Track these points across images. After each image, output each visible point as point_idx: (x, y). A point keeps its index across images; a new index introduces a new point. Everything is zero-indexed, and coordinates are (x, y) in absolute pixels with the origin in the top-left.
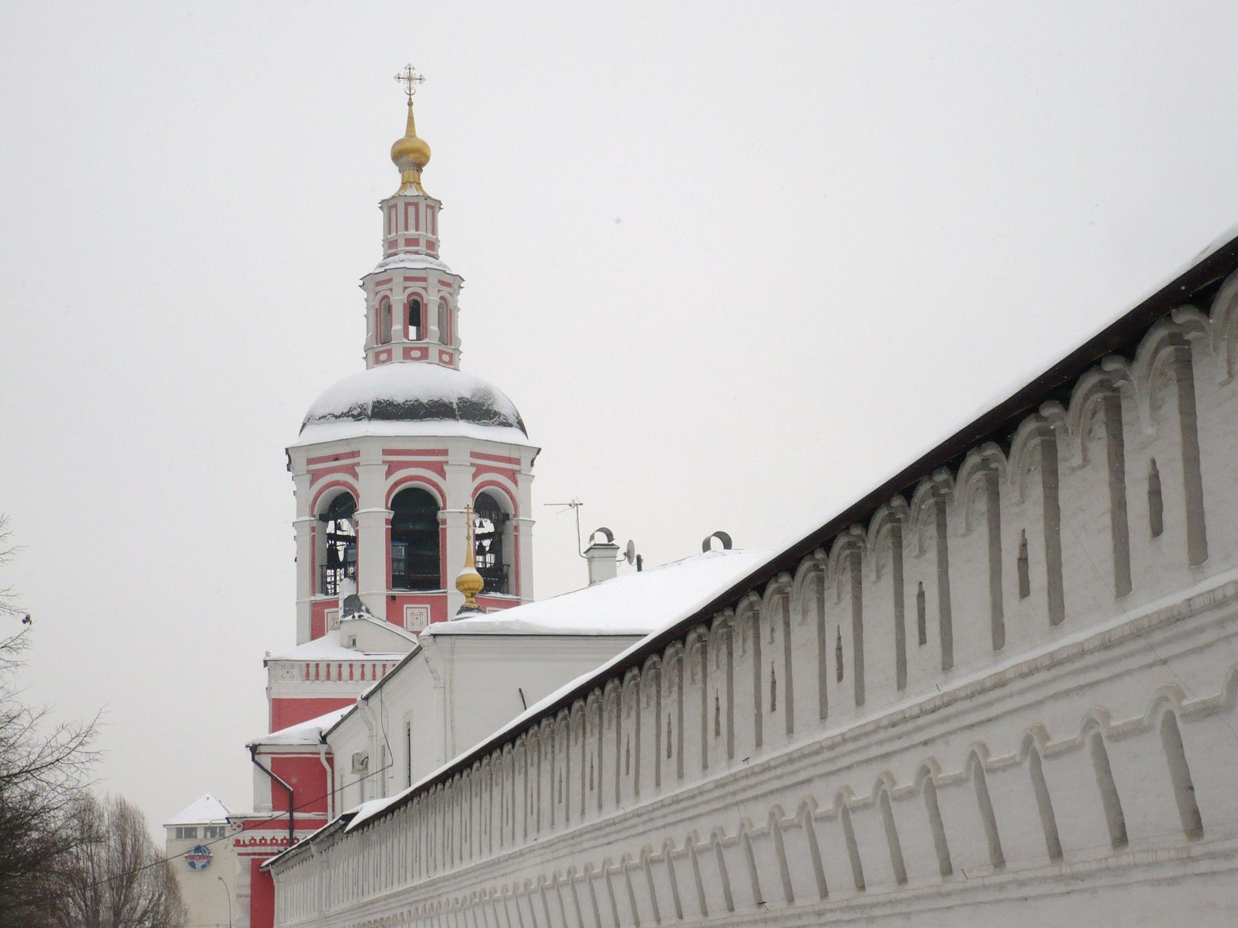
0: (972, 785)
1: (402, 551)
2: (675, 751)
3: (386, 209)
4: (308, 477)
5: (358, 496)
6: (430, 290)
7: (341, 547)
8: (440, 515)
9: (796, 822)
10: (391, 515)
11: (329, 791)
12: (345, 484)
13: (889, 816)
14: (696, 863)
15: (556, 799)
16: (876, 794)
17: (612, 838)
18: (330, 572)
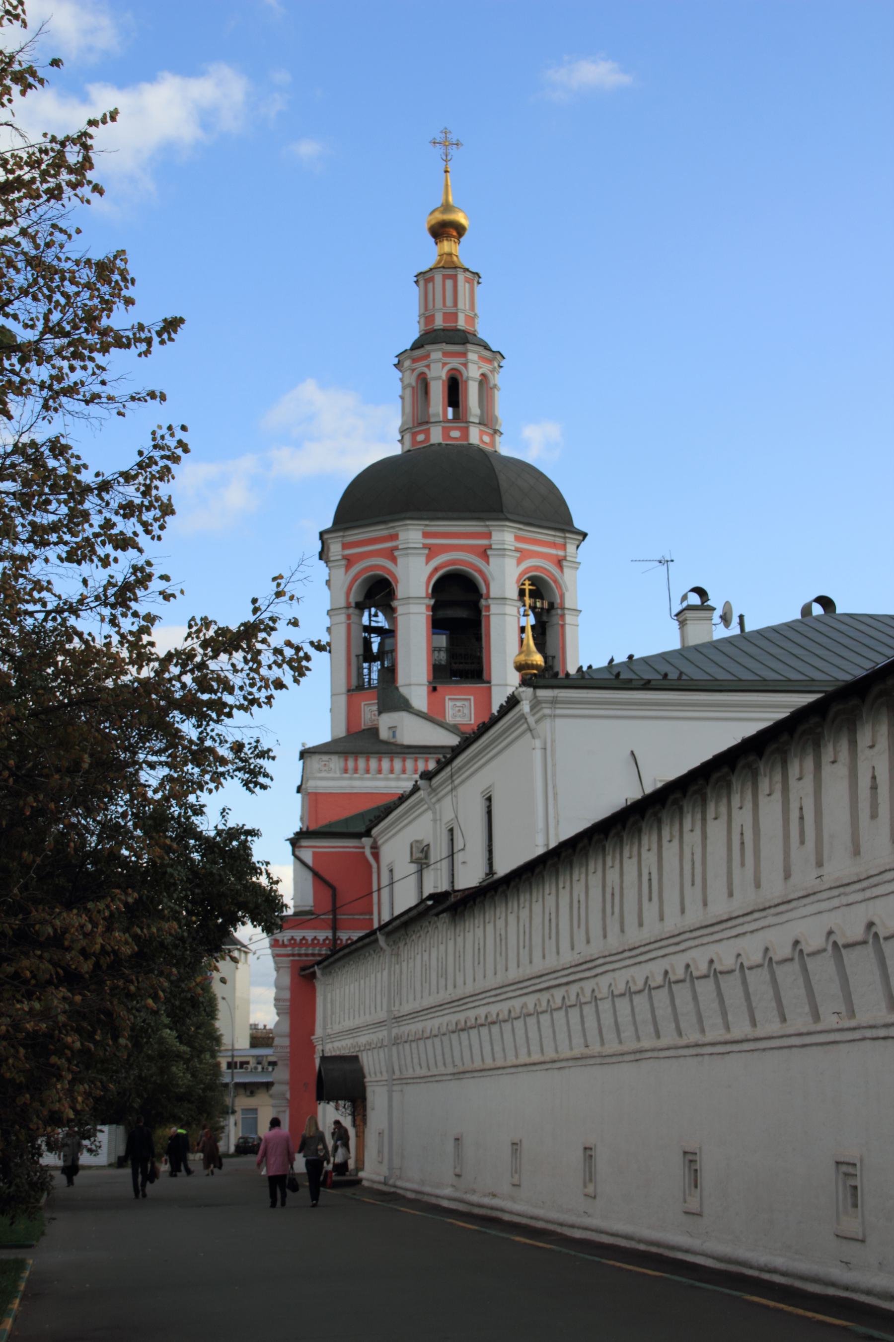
0: (593, 1004)
1: (442, 640)
2: (503, 954)
3: (422, 283)
4: (344, 562)
5: (397, 581)
6: (470, 365)
7: (376, 641)
8: (483, 602)
9: (790, 957)
10: (432, 602)
11: (375, 887)
12: (383, 568)
13: (772, 973)
14: (650, 998)
15: (476, 962)
16: (665, 981)
17: (705, 940)
18: (366, 665)
